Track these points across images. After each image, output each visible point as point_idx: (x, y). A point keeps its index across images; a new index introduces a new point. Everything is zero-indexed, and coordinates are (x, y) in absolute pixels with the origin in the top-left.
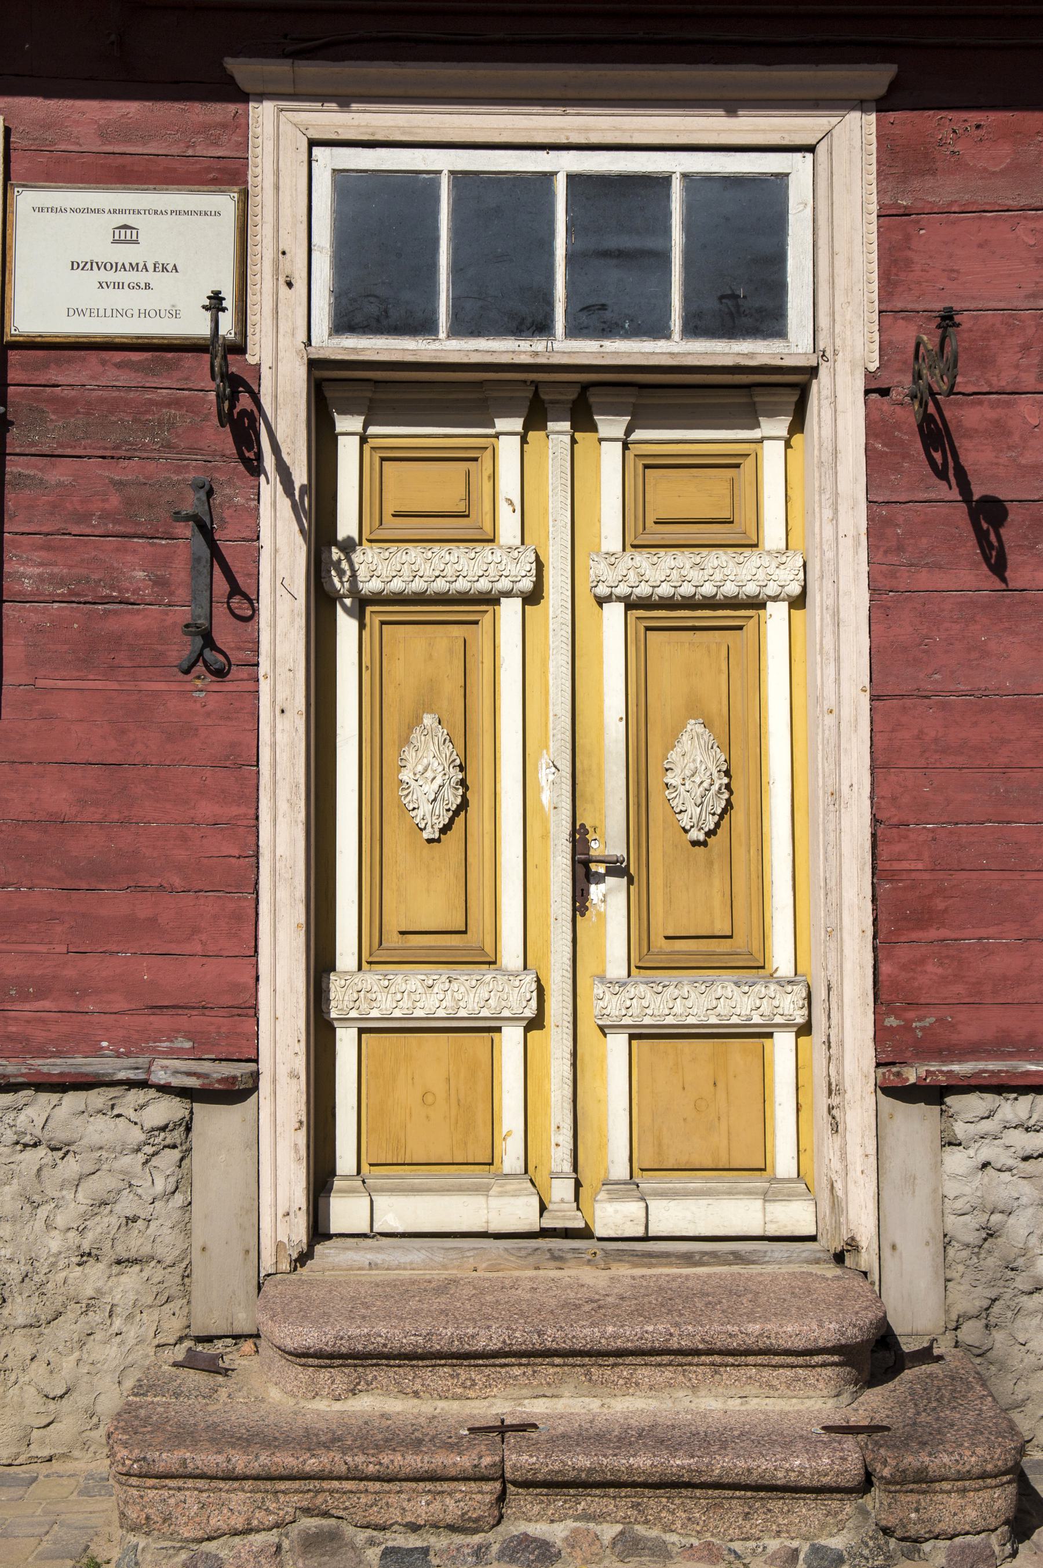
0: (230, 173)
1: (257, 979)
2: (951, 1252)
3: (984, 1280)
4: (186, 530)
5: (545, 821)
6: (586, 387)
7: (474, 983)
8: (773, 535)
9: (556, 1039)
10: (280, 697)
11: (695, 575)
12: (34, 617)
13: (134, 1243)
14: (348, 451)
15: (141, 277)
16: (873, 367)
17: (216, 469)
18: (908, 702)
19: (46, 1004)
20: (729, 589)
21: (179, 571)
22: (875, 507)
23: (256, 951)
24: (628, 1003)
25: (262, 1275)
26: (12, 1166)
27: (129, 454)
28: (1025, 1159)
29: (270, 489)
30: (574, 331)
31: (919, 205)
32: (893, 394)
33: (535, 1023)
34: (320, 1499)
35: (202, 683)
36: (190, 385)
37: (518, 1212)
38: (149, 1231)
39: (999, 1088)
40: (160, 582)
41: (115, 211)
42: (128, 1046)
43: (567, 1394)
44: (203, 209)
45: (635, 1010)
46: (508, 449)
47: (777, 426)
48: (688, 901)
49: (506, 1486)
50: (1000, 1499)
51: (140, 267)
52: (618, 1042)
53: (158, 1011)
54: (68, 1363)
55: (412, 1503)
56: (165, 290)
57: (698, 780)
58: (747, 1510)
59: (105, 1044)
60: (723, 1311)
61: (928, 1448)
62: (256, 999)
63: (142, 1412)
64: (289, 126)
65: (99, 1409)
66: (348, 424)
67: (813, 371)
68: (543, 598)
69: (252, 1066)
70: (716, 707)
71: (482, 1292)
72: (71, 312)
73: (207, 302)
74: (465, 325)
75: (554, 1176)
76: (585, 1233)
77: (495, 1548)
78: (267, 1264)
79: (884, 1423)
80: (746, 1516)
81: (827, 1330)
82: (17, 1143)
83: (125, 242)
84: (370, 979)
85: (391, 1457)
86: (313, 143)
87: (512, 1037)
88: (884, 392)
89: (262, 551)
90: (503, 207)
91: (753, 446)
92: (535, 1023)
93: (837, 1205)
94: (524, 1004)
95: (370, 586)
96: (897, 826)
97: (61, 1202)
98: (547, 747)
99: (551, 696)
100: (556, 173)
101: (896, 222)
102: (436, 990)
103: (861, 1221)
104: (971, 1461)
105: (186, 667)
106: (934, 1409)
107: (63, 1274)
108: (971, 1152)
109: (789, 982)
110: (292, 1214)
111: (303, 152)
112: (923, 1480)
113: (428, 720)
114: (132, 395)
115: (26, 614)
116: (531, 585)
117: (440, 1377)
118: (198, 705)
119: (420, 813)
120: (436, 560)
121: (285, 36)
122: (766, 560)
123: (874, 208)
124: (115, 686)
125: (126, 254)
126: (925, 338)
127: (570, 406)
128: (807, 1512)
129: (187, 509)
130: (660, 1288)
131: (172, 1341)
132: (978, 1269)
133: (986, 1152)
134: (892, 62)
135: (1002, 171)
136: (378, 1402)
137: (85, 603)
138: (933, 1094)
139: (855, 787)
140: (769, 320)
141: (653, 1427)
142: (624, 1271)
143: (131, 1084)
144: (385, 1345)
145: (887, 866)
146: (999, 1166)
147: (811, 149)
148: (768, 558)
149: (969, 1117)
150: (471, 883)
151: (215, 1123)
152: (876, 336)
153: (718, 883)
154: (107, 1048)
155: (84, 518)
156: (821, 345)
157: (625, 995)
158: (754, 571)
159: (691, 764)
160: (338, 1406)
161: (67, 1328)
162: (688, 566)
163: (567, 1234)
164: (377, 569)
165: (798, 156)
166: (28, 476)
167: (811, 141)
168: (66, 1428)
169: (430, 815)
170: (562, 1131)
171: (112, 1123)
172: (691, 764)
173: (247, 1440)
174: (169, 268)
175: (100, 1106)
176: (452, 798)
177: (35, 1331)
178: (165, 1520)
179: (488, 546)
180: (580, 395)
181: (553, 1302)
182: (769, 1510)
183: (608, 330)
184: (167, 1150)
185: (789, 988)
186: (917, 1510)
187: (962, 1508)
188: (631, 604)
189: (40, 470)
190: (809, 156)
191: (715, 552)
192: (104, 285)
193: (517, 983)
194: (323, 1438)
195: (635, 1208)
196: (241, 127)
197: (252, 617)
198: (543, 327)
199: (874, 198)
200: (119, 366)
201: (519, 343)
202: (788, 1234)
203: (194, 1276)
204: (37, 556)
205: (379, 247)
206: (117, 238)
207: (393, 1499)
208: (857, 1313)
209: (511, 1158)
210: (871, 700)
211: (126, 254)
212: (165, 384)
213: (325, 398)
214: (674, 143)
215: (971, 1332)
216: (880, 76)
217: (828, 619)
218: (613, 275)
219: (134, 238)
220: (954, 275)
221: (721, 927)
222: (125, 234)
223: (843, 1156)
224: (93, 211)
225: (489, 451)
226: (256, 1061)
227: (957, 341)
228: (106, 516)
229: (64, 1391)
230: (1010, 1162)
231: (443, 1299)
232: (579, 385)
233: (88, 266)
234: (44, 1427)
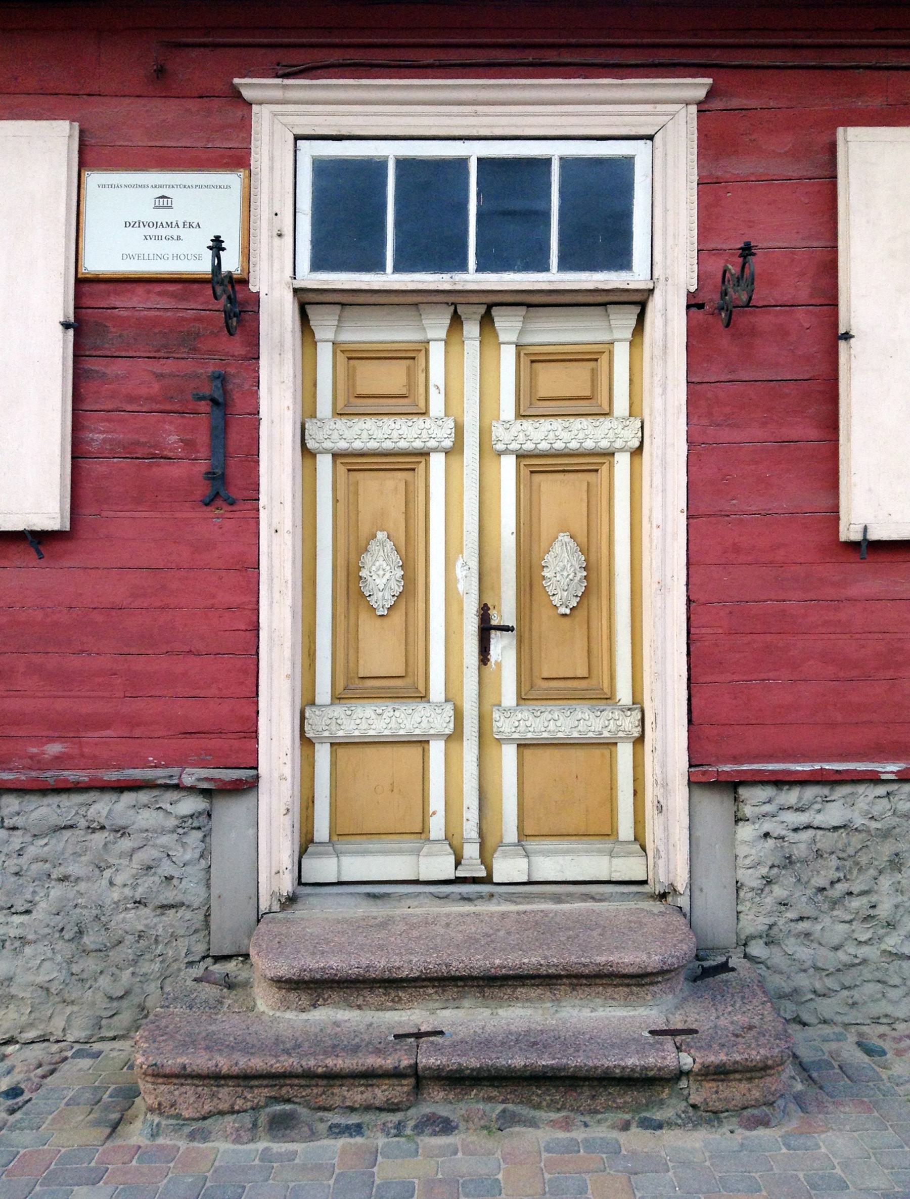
1: (258, 712)
2: (742, 894)
3: (764, 912)
4: (204, 406)
5: (461, 602)
6: (490, 307)
7: (410, 711)
10: (275, 521)
11: (566, 436)
13: (169, 896)
15: (174, 232)
16: (693, 289)
17: (228, 365)
18: (712, 519)
19: (108, 733)
20: (589, 444)
23: (257, 694)
24: (517, 724)
25: (260, 914)
26: (86, 843)
27: (166, 355)
28: (796, 830)
31: (728, 176)
32: (707, 307)
34: (284, 1091)
35: (218, 513)
36: (210, 307)
38: (181, 886)
40: (189, 444)
43: (467, 1005)
44: (218, 184)
45: (522, 728)
48: (562, 658)
53: (187, 736)
54: (126, 975)
55: (351, 1093)
57: (565, 574)
58: (594, 1093)
59: (151, 759)
60: (580, 945)
61: (725, 1050)
62: (257, 726)
63: (163, 1022)
64: (280, 126)
65: (147, 1004)
67: (651, 291)
69: (253, 772)
71: (412, 927)
72: (125, 257)
73: (211, 244)
75: (469, 841)
77: (411, 1123)
78: (263, 907)
79: (694, 1027)
80: (593, 1097)
82: (89, 827)
83: (164, 207)
84: (338, 711)
85: (335, 1062)
86: (297, 138)
88: (700, 306)
89: (262, 422)
91: (607, 346)
94: (445, 725)
96: (704, 604)
97: (119, 867)
98: (462, 553)
100: (470, 157)
101: (709, 187)
102: (384, 716)
105: (207, 500)
106: (730, 1013)
107: (121, 916)
108: (757, 826)
109: (629, 709)
110: (281, 873)
113: (381, 535)
114: (169, 314)
116: (451, 444)
118: (216, 527)
119: (374, 598)
120: (385, 427)
121: (278, 65)
122: (615, 424)
123: (696, 178)
124: (159, 515)
125: (163, 216)
126: (730, 267)
129: (206, 391)
130: (537, 923)
131: (197, 959)
132: (760, 905)
133: (767, 826)
135: (786, 153)
137: (137, 458)
138: (732, 786)
139: (675, 578)
140: (620, 258)
141: (528, 1032)
143: (167, 787)
144: (336, 975)
146: (775, 835)
147: (651, 138)
148: (616, 423)
149: (754, 802)
150: (414, 641)
151: (231, 811)
152: (696, 266)
153: (580, 644)
155: (131, 399)
156: (655, 276)
157: (513, 719)
158: (607, 431)
160: (304, 1016)
161: (126, 952)
162: (560, 429)
163: (475, 881)
165: (641, 143)
167: (650, 132)
170: (471, 810)
171: (154, 813)
172: (561, 569)
173: (233, 1047)
175: (146, 802)
176: (397, 587)
177: (102, 954)
178: (172, 1106)
179: (422, 418)
181: (460, 937)
182: (610, 1093)
184: (194, 831)
185: (629, 713)
186: (717, 1092)
187: (750, 1090)
188: (521, 456)
190: (649, 142)
191: (579, 420)
193: (440, 711)
194: (288, 1046)
195: (523, 863)
199: (696, 171)
200: (159, 294)
201: (443, 275)
202: (627, 879)
203: (212, 916)
204: (102, 426)
205: (346, 211)
207: (336, 1090)
208: (675, 946)
211: (163, 216)
217: (657, 462)
220: (751, 224)
221: (582, 672)
223: (666, 829)
225: (423, 352)
226: (256, 768)
227: (756, 264)
228: (150, 399)
229: (122, 994)
230: (783, 833)
231: (383, 934)
233: (137, 225)
234: (110, 1017)
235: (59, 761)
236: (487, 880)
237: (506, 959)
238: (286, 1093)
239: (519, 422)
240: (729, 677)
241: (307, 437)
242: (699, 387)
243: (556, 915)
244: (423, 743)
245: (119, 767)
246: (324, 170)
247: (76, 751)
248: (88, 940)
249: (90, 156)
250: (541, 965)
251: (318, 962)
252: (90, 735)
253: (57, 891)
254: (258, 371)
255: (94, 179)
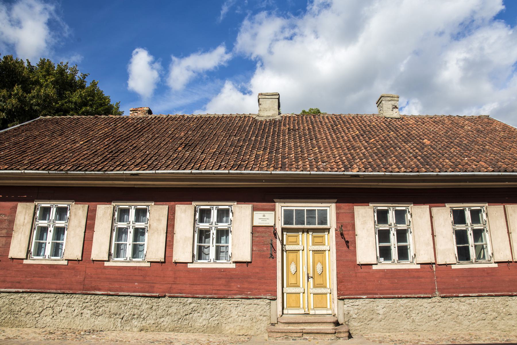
0: (274, 210)
8: (327, 244)
9: (306, 294)
13: (265, 314)
14: (285, 236)
21: (269, 248)
29: (278, 240)
30: (307, 224)
33: (304, 293)
35: (271, 259)
37: (303, 312)
39: (349, 299)
42: (265, 295)
46: (300, 235)
47: (327, 233)
48: (319, 281)
49: (303, 333)
50: (347, 334)
52: (312, 295)
56: (268, 221)
66: (285, 233)
70: (321, 261)
74: (296, 224)
76: (309, 314)
81: (332, 321)
84: (288, 288)
87: (301, 294)
90: (300, 213)
92: (304, 293)
93: (334, 311)
95: (287, 249)
99: (305, 260)
101: (338, 214)
103: (336, 312)
104: (344, 331)
111: (281, 207)
112: (340, 332)
117: (296, 325)
128: (330, 336)
136: (291, 327)
138: (343, 299)
140: (325, 223)
142: (313, 317)
150: (297, 279)
153: (322, 279)
159: (319, 267)
161: (259, 322)
164: (288, 247)
168: (259, 332)
169: (293, 272)
172: (319, 267)
183: (310, 224)
195: (314, 311)
196: (275, 205)
197: (276, 253)
198: (304, 224)
205: (288, 217)
209: (302, 306)
212: (268, 230)
214: (316, 206)
215: (347, 323)
216: (336, 200)
218: (310, 219)
222: (264, 216)
238: (286, 334)
246: (285, 210)
248: (254, 320)
249: (254, 209)
253: (249, 313)
255: (255, 212)
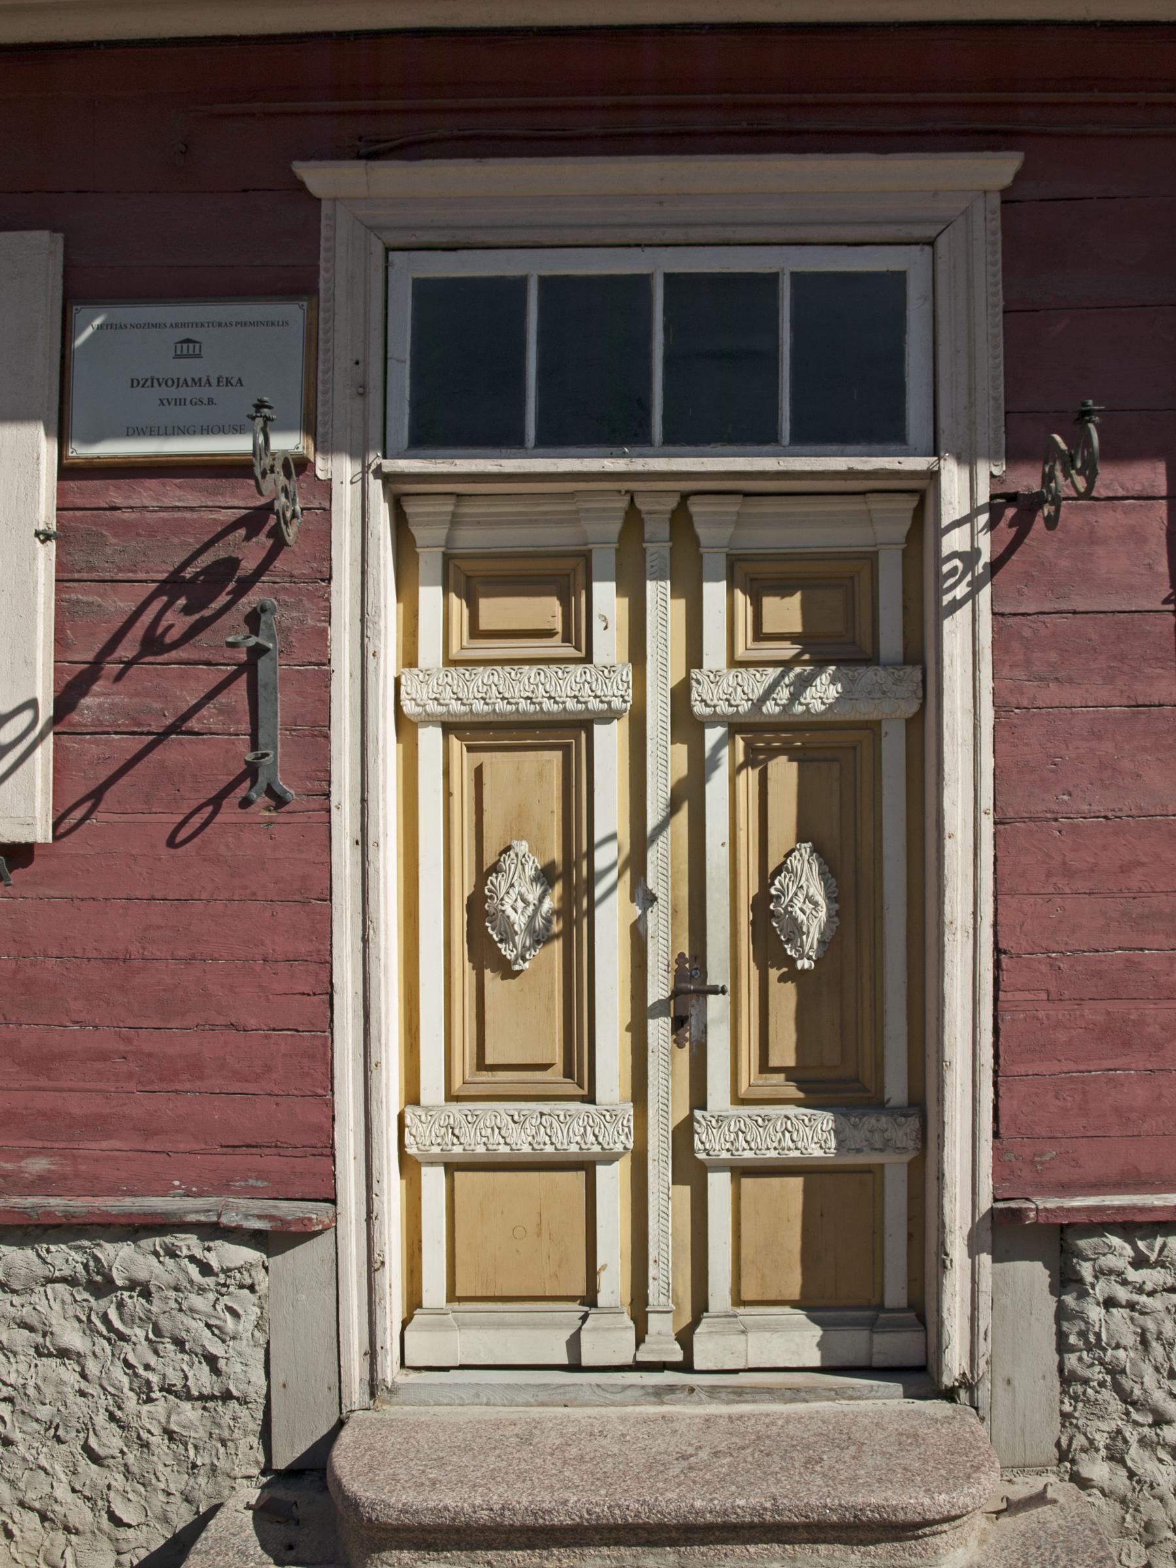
6: (685, 496)
12: (94, 750)
15: (204, 392)
22: (1000, 619)
41: (177, 325)
51: (204, 381)
53: (229, 1150)
59: (177, 1183)
68: (628, 1029)
86: (388, 250)
101: (1017, 314)
115: (86, 745)
121: (360, 139)
127: (668, 516)
134: (1017, 149)
145: (1009, 996)
154: (179, 1187)
166: (88, 604)
167: (929, 232)
174: (234, 381)
180: (679, 504)
189: (100, 596)
192: (165, 402)
206: (179, 352)
210: (995, 823)
213: (404, 513)
219: (197, 352)
222: (188, 348)
224: (154, 326)
232: (679, 494)
233: (149, 383)
235: (42, 1184)
236: (686, 1366)
237: (712, 1500)
239: (733, 671)
240: (1055, 1067)
241: (403, 695)
242: (1011, 621)
243: (787, 1422)
244: (586, 1166)
245: (132, 1194)
247: (69, 1170)
250: (765, 1509)
251: (425, 1500)
252: (88, 1146)
254: (328, 600)
